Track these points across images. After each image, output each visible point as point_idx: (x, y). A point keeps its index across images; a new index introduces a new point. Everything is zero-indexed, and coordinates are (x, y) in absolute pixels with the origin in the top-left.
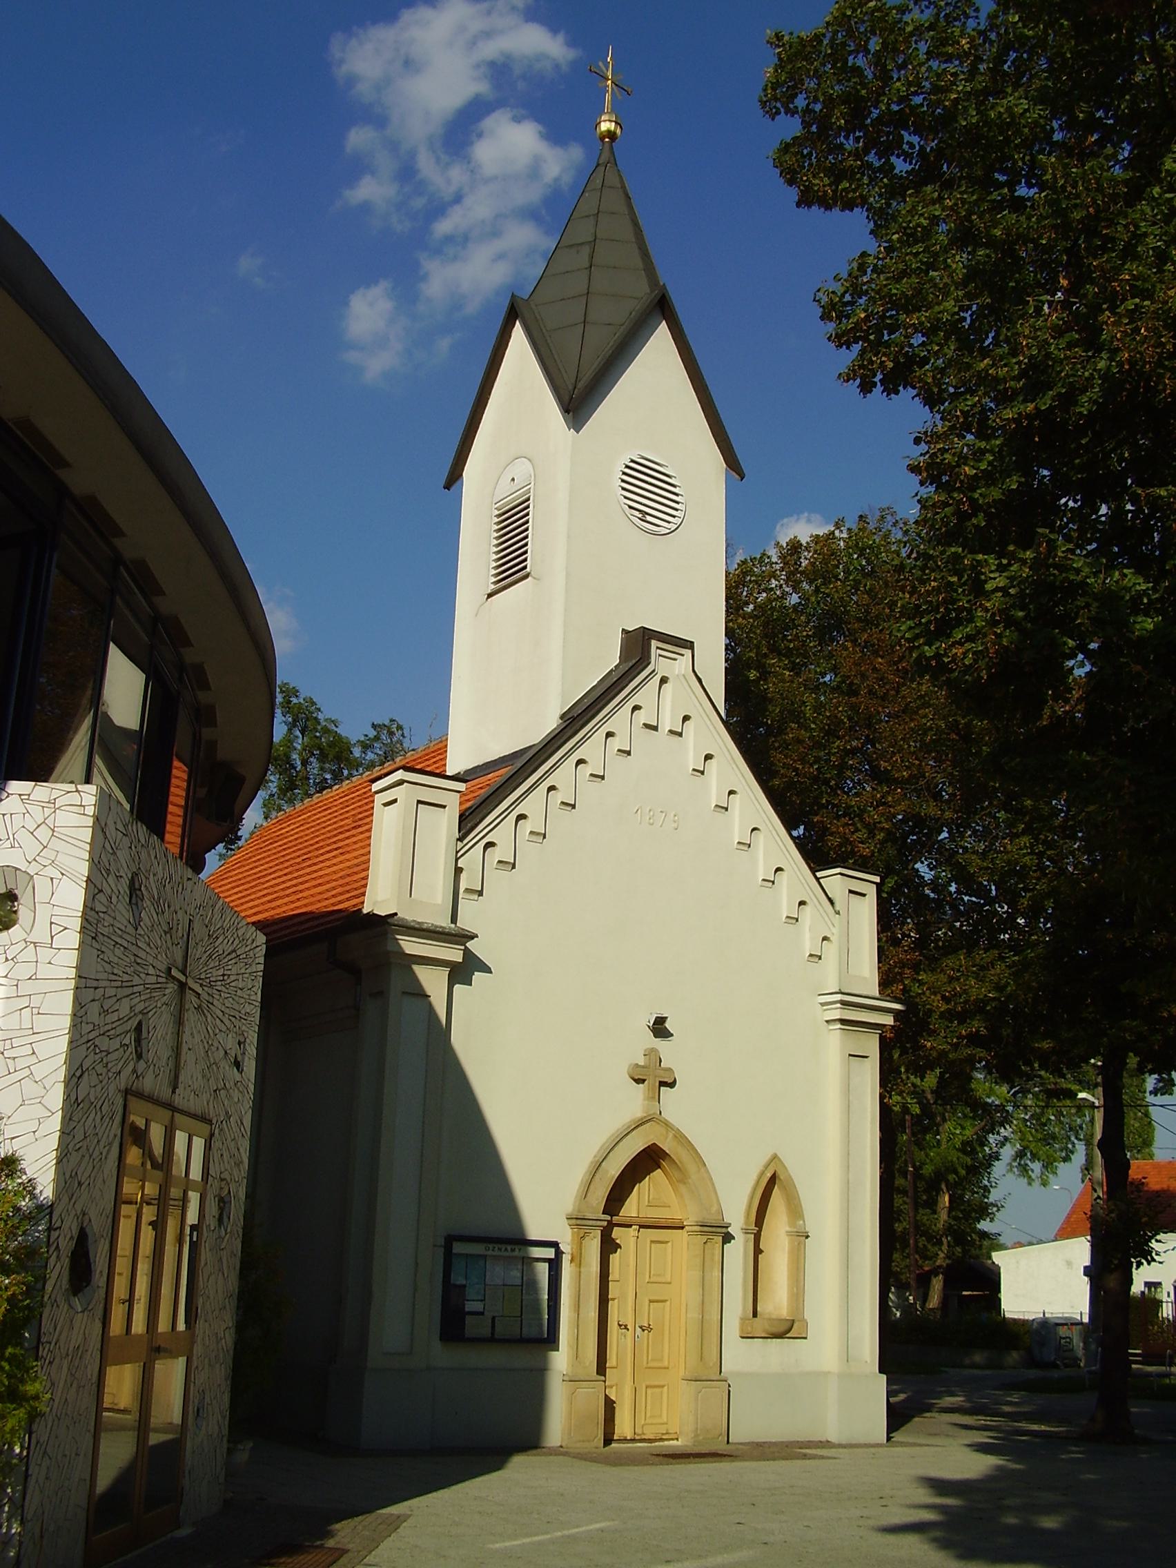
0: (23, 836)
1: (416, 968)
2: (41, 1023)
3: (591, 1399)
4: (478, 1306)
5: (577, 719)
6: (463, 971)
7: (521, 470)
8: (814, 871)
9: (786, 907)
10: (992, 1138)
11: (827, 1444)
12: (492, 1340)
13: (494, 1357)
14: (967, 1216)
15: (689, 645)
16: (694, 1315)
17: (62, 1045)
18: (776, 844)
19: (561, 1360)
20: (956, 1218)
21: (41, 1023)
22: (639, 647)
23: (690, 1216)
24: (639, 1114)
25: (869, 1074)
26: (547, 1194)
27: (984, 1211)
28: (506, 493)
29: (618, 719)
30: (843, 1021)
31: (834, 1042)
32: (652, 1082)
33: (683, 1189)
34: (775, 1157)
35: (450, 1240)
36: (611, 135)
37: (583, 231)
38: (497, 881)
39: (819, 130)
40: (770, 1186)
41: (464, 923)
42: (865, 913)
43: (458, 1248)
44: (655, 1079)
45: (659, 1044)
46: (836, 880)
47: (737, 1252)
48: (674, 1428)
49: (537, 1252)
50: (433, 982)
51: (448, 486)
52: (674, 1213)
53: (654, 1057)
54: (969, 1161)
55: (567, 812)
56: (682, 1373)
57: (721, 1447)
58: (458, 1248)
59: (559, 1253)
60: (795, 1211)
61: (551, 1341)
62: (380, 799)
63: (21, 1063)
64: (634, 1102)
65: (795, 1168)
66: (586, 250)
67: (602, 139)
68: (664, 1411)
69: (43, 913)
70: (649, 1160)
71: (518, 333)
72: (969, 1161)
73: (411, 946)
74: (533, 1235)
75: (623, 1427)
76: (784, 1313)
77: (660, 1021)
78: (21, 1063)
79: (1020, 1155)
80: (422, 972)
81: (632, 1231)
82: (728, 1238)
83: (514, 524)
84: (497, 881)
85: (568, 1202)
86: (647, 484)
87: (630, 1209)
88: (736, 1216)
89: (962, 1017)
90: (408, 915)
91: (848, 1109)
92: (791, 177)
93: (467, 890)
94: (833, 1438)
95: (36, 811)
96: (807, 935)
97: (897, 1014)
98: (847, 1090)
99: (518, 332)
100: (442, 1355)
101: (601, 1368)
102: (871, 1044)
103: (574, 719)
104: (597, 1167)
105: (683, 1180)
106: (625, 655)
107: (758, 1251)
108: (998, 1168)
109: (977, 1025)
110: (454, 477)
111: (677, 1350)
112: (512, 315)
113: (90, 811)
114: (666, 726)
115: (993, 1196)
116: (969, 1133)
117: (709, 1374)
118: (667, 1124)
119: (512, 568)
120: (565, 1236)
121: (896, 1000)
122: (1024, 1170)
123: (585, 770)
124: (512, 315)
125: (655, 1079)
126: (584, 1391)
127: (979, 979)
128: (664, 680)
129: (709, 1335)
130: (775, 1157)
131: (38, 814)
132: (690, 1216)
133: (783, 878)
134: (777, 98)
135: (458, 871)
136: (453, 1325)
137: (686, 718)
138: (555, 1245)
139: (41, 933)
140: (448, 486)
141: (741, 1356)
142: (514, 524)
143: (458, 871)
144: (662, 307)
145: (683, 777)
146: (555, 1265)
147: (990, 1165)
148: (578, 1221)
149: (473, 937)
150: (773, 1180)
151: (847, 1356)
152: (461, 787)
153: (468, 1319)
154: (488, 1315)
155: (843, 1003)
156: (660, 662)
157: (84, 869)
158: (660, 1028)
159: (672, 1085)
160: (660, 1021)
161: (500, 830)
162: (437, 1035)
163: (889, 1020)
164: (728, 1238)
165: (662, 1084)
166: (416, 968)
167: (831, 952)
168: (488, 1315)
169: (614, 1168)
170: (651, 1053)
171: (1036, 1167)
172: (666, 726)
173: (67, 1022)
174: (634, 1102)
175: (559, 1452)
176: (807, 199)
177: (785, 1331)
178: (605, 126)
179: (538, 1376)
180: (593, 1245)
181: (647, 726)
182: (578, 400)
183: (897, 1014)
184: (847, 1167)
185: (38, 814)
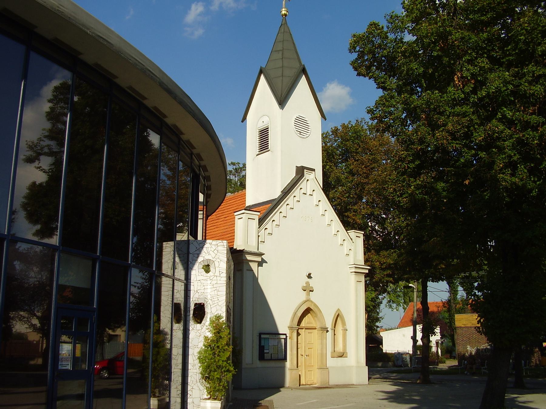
0: (211, 252)
1: (250, 263)
2: (219, 293)
3: (295, 373)
4: (267, 351)
5: (287, 192)
6: (260, 264)
7: (266, 119)
8: (347, 230)
9: (340, 241)
10: (380, 297)
11: (353, 385)
12: (271, 359)
13: (272, 364)
14: (373, 321)
15: (314, 170)
16: (320, 352)
17: (224, 298)
18: (337, 224)
19: (288, 364)
20: (369, 322)
21: (219, 293)
22: (301, 171)
23: (318, 326)
24: (305, 299)
25: (362, 286)
26: (283, 322)
27: (378, 320)
28: (262, 126)
29: (296, 192)
30: (355, 272)
31: (353, 277)
32: (308, 290)
33: (316, 318)
34: (339, 309)
35: (260, 334)
36: (285, 15)
37: (279, 47)
38: (268, 239)
39: (361, 55)
40: (338, 316)
41: (261, 250)
42: (360, 242)
43: (263, 336)
44: (308, 290)
45: (309, 280)
46: (352, 233)
47: (330, 335)
48: (315, 381)
49: (282, 337)
50: (254, 266)
51: (242, 122)
52: (313, 325)
53: (307, 283)
54: (374, 304)
55: (284, 218)
56: (317, 367)
57: (328, 386)
58: (263, 336)
59: (286, 337)
60: (344, 324)
61: (285, 359)
62: (237, 217)
63: (215, 302)
64: (303, 296)
65: (344, 313)
66: (281, 52)
67: (283, 16)
68: (313, 377)
69: (217, 269)
70: (308, 311)
71: (262, 77)
72: (374, 304)
73: (249, 257)
74: (280, 332)
75: (303, 382)
76: (341, 351)
77: (310, 274)
78: (215, 302)
79: (389, 302)
80: (251, 264)
81: (303, 330)
82: (327, 331)
83: (264, 134)
84: (268, 239)
85: (288, 324)
86: (301, 124)
87: (303, 324)
88: (329, 325)
89: (384, 270)
90: (247, 249)
91: (357, 296)
92: (355, 69)
93: (261, 242)
94: (355, 383)
95: (213, 246)
96: (345, 249)
97: (369, 270)
98: (356, 290)
99: (262, 77)
100: (259, 364)
101: (297, 367)
102: (363, 278)
103: (286, 193)
104: (295, 314)
105: (316, 316)
106: (297, 173)
107: (335, 334)
108: (382, 306)
109: (389, 272)
110: (244, 119)
111: (315, 361)
112: (261, 72)
113: (226, 246)
114: (308, 193)
115: (381, 315)
116: (373, 295)
117: (324, 368)
118: (312, 302)
119: (264, 146)
120: (287, 332)
121: (369, 266)
122: (391, 307)
123: (289, 207)
124: (261, 72)
125: (308, 290)
126: (294, 372)
127: (389, 257)
128: (308, 180)
129: (323, 356)
130: (339, 309)
131: (214, 247)
132: (318, 326)
133: (339, 233)
134: (352, 49)
135: (259, 236)
136: (262, 357)
137: (314, 191)
138: (285, 334)
139: (217, 274)
140: (242, 122)
141: (331, 362)
142: (264, 134)
143: (259, 236)
144: (304, 71)
145: (312, 206)
146: (286, 339)
147: (379, 305)
148: (291, 328)
149: (263, 254)
150: (338, 316)
151: (358, 362)
152: (259, 214)
153: (265, 354)
154: (270, 353)
155: (355, 267)
156: (307, 175)
157: (226, 259)
158: (309, 276)
159: (312, 291)
160: (310, 274)
161: (268, 224)
162: (255, 279)
163: (367, 271)
164: (327, 331)
165: (311, 291)
166: (250, 263)
167: (351, 253)
168: (270, 353)
169: (299, 314)
170: (307, 283)
171: (394, 305)
172: (308, 193)
173: (225, 293)
174: (303, 296)
175: (289, 388)
176: (359, 74)
177: (342, 355)
178: (283, 12)
179: (283, 368)
180: (295, 334)
181: (304, 193)
182: (282, 101)
183: (369, 270)
184: (357, 312)
185: (214, 247)
